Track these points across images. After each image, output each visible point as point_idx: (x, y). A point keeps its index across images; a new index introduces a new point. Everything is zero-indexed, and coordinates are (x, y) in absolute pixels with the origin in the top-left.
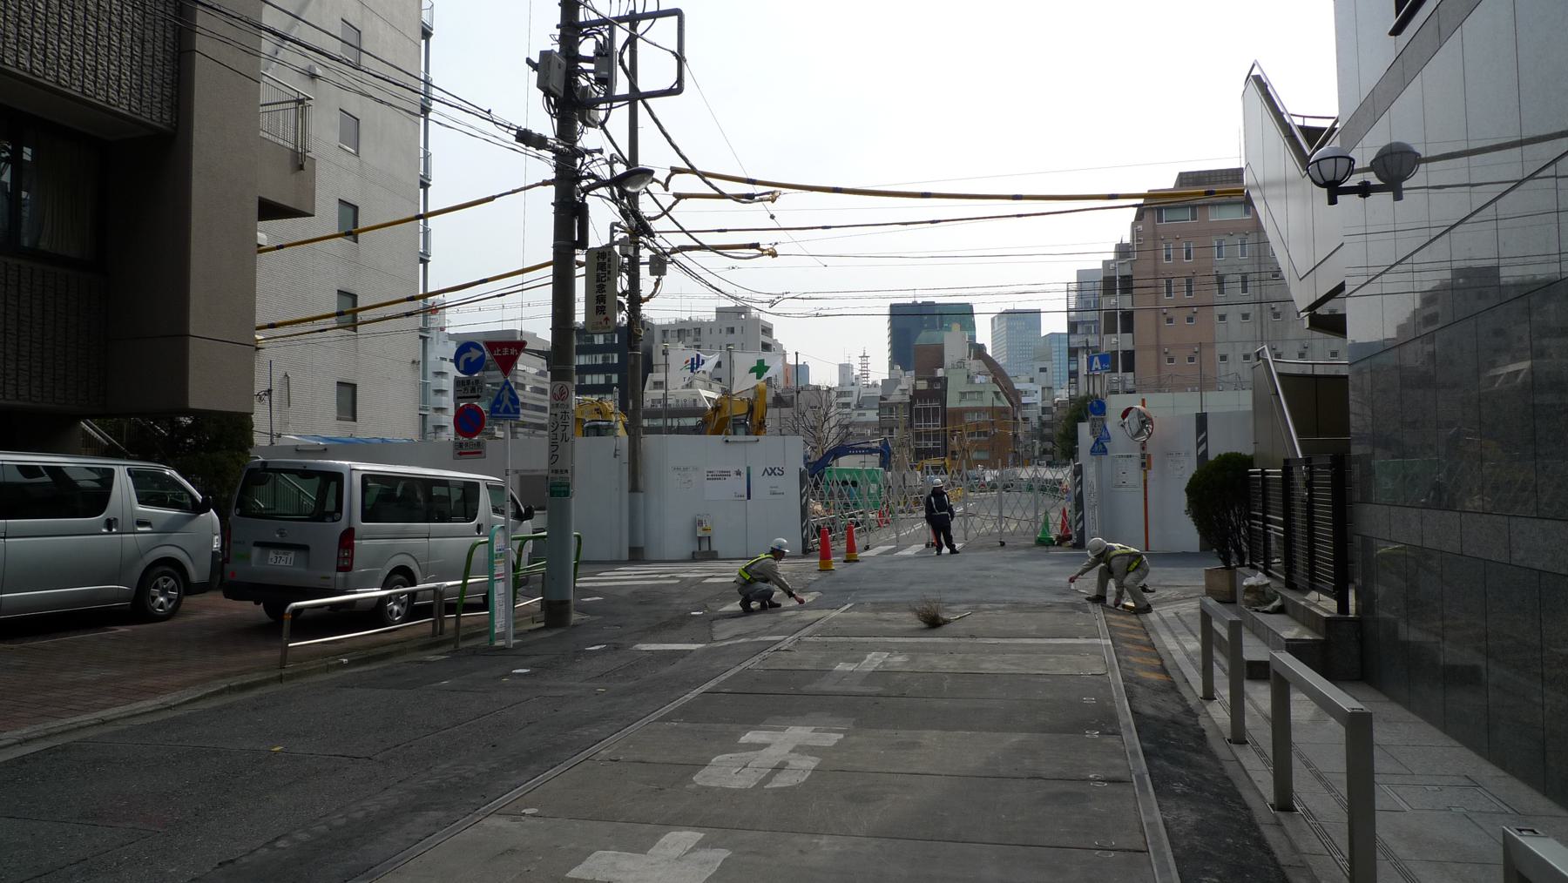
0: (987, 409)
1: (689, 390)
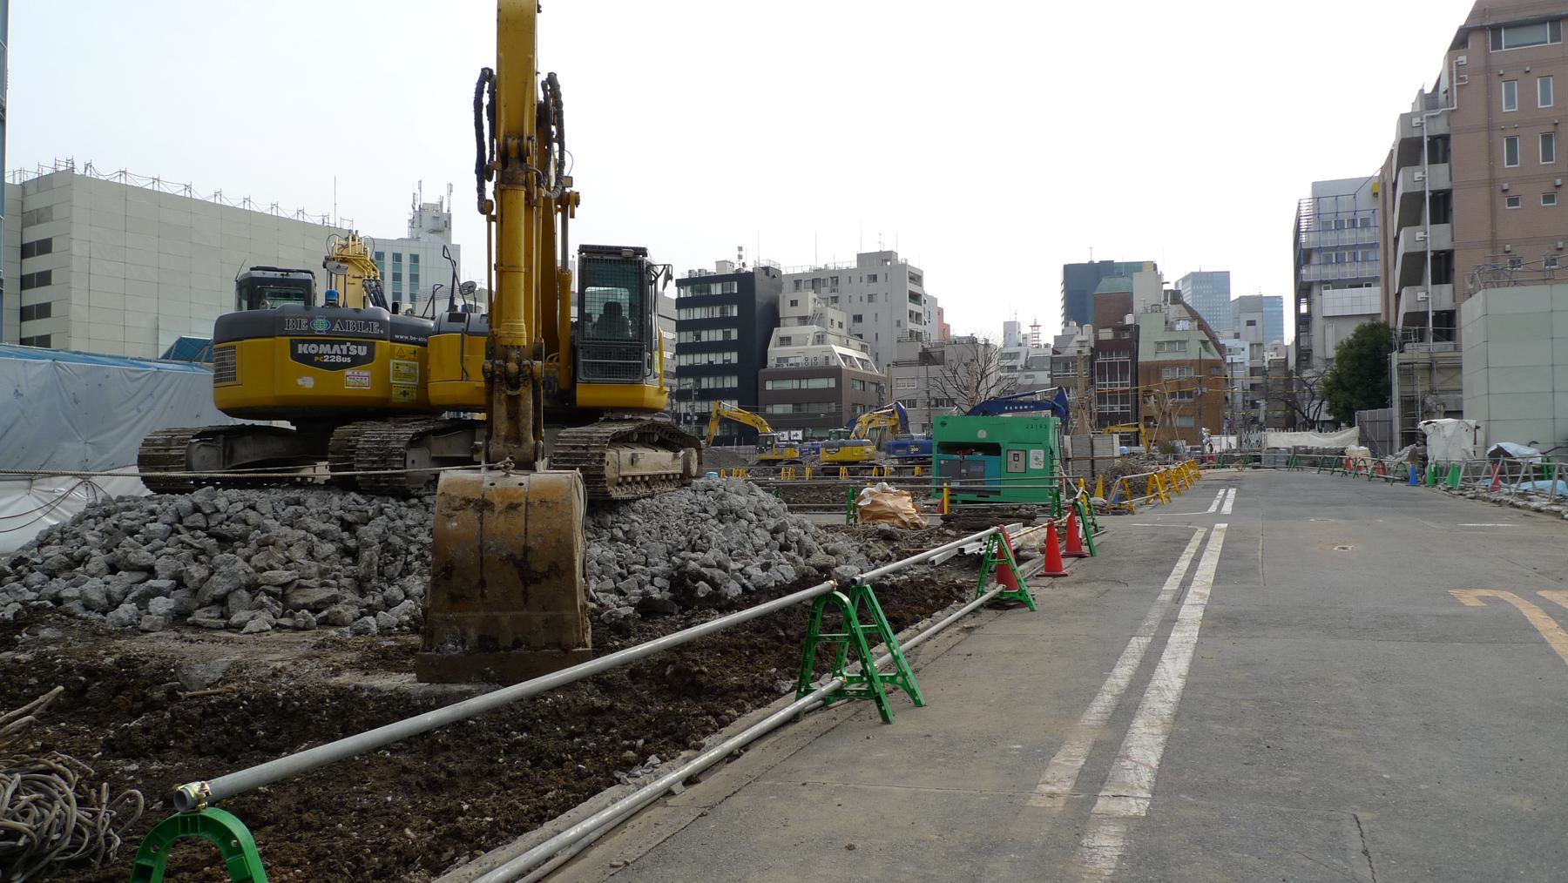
0: (1192, 363)
1: (819, 346)
